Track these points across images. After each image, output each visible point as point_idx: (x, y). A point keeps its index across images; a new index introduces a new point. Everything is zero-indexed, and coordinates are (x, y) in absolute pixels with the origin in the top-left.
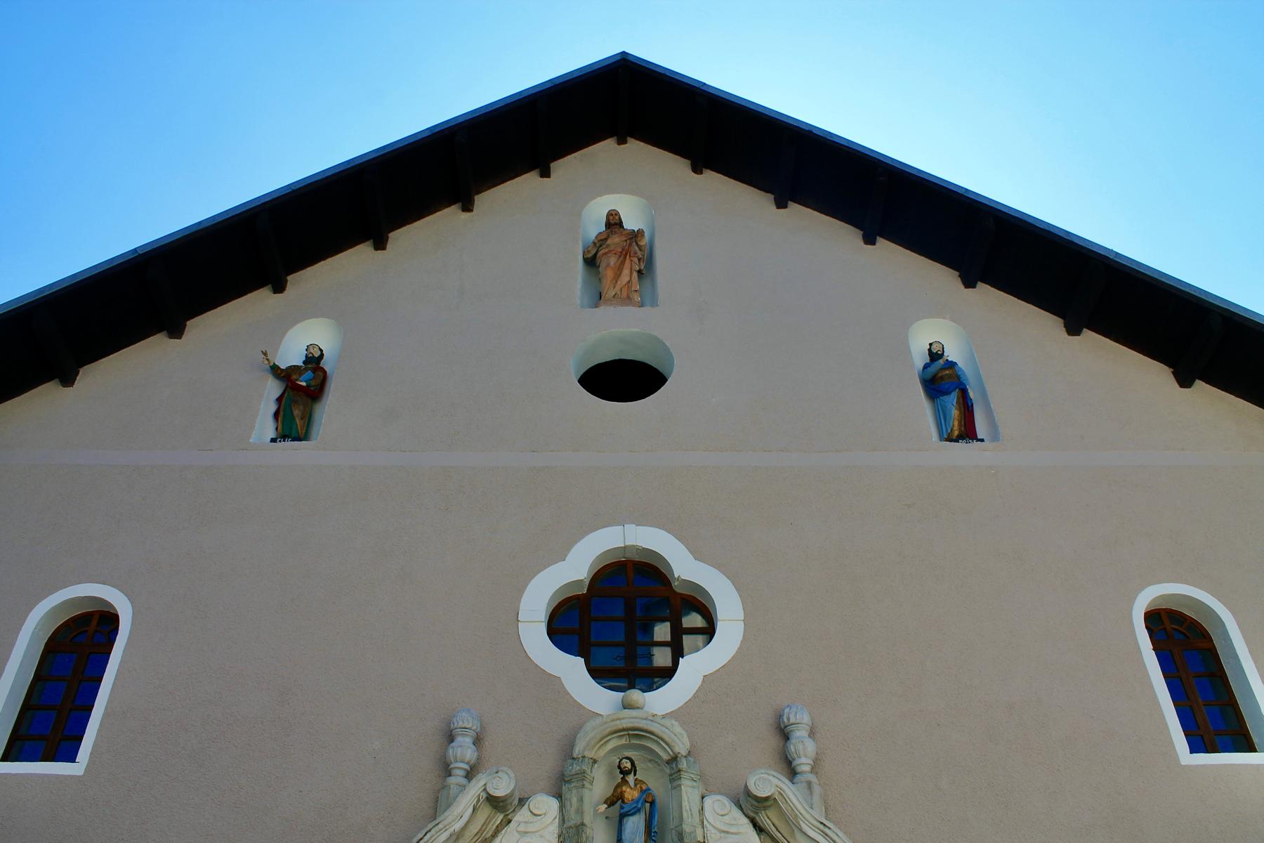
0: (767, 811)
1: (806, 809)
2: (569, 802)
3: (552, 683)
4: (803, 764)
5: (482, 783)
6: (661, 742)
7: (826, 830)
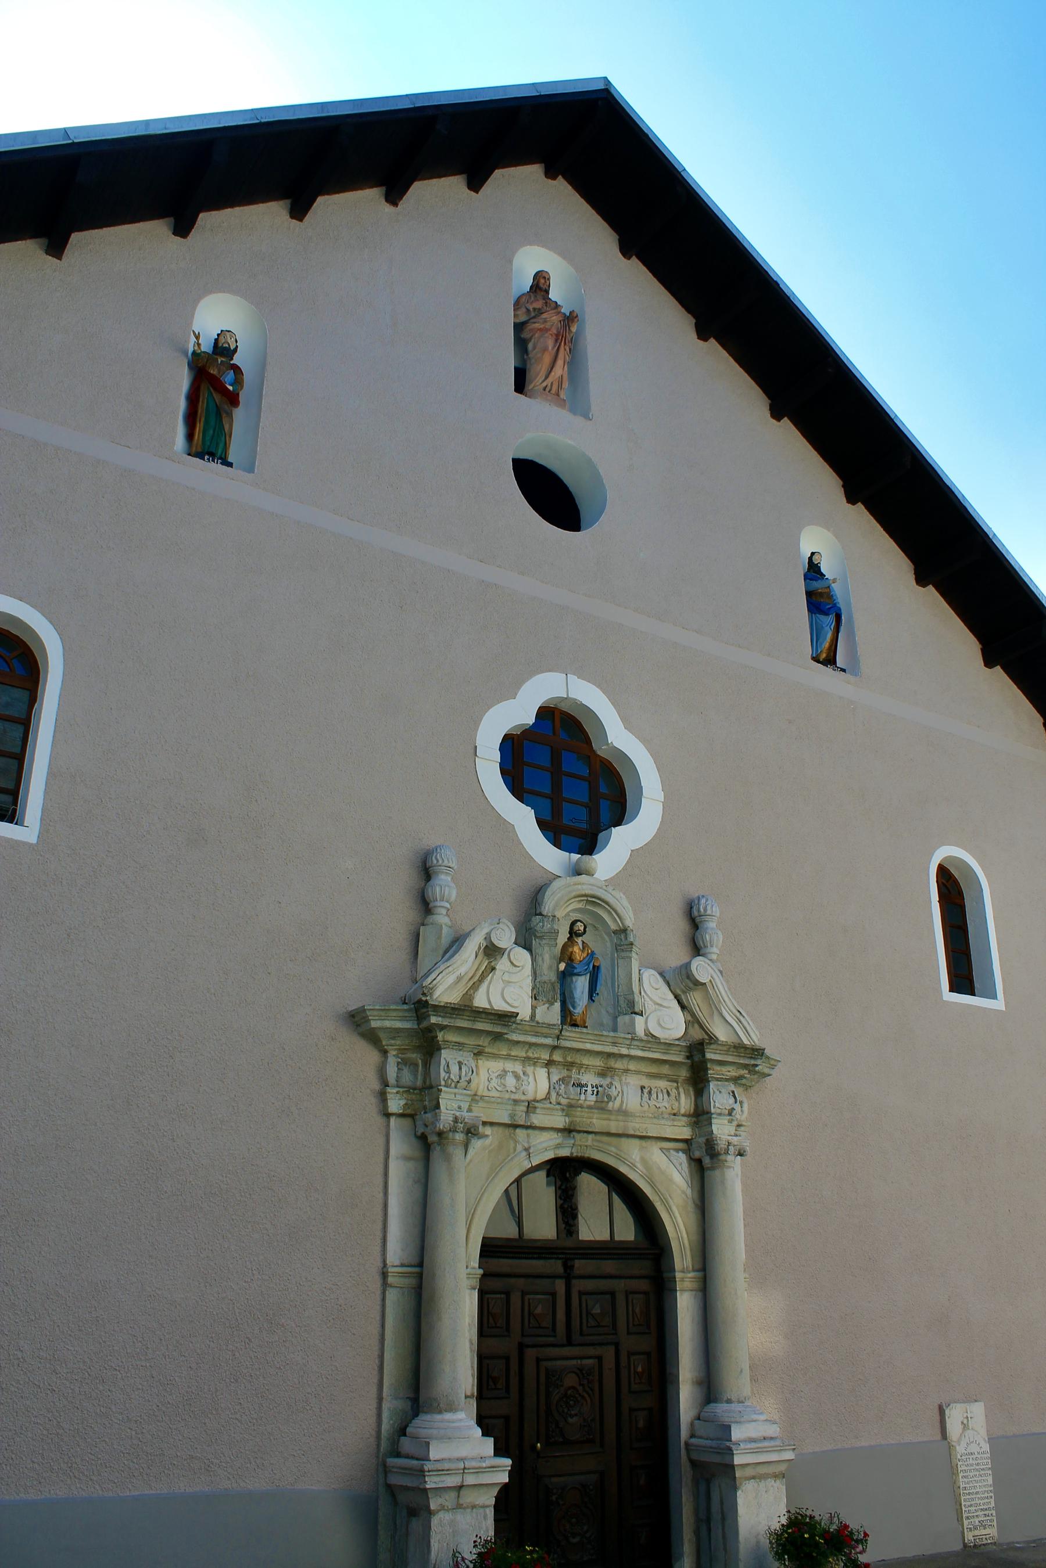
0: (694, 993)
1: (728, 996)
2: (540, 959)
3: (506, 829)
4: (714, 953)
5: (486, 931)
6: (613, 913)
7: (741, 1018)
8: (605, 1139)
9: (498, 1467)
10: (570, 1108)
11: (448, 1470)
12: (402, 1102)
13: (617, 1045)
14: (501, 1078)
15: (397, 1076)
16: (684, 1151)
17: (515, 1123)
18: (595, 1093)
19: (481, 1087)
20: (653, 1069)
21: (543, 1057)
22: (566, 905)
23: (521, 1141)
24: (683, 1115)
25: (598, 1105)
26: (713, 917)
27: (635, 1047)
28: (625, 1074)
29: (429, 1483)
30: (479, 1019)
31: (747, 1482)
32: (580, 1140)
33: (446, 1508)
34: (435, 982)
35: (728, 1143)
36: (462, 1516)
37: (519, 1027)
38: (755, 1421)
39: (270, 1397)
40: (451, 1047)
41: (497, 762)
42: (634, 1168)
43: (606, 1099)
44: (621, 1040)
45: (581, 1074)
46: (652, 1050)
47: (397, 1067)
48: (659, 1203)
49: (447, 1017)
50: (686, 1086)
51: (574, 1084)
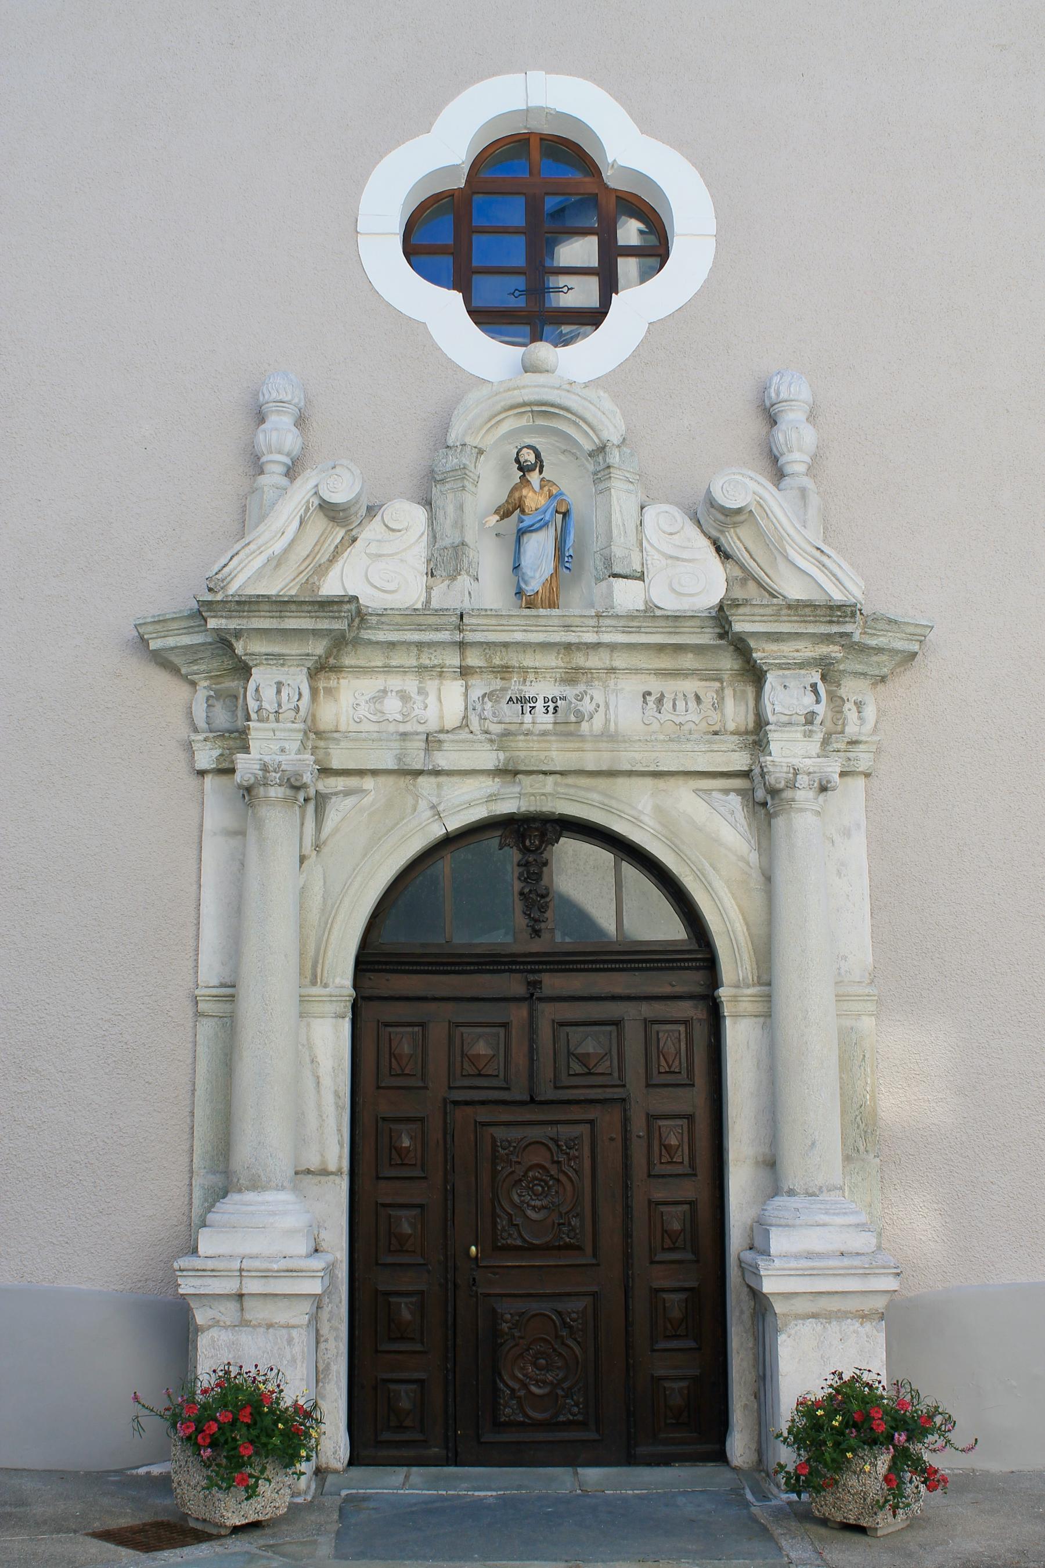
0: (738, 530)
5: (311, 483)
7: (824, 559)
8: (584, 781)
9: (302, 1271)
10: (503, 739)
11: (213, 1270)
12: (216, 753)
13: (572, 629)
14: (375, 703)
15: (207, 716)
16: (738, 792)
17: (406, 767)
18: (551, 709)
19: (343, 720)
20: (665, 662)
21: (448, 663)
22: (489, 425)
23: (425, 794)
24: (733, 733)
25: (559, 728)
26: (794, 403)
27: (609, 629)
28: (613, 676)
29: (182, 1286)
30: (288, 614)
31: (800, 1321)
32: (531, 786)
33: (222, 1324)
34: (226, 570)
35: (794, 769)
36: (250, 1337)
37: (383, 619)
38: (824, 1225)
39: (19, 1165)
40: (265, 662)
41: (395, 234)
42: (639, 824)
43: (573, 719)
44: (577, 621)
45: (528, 683)
46: (643, 630)
47: (206, 703)
48: (691, 878)
49: (235, 617)
50: (740, 686)
51: (511, 699)
